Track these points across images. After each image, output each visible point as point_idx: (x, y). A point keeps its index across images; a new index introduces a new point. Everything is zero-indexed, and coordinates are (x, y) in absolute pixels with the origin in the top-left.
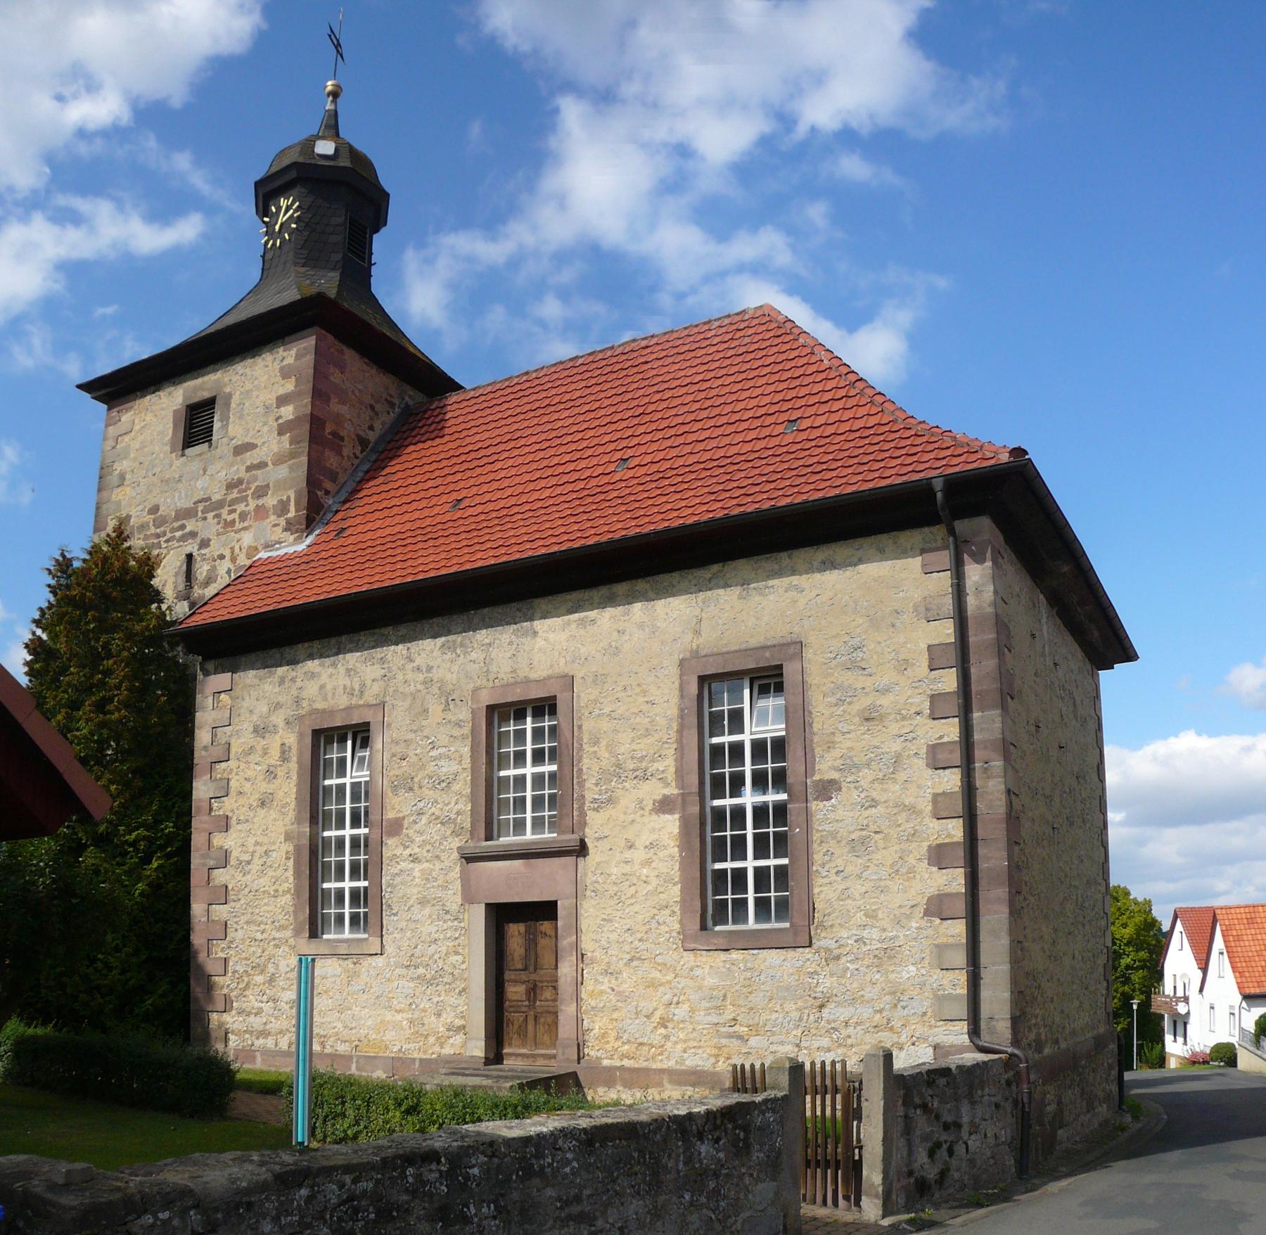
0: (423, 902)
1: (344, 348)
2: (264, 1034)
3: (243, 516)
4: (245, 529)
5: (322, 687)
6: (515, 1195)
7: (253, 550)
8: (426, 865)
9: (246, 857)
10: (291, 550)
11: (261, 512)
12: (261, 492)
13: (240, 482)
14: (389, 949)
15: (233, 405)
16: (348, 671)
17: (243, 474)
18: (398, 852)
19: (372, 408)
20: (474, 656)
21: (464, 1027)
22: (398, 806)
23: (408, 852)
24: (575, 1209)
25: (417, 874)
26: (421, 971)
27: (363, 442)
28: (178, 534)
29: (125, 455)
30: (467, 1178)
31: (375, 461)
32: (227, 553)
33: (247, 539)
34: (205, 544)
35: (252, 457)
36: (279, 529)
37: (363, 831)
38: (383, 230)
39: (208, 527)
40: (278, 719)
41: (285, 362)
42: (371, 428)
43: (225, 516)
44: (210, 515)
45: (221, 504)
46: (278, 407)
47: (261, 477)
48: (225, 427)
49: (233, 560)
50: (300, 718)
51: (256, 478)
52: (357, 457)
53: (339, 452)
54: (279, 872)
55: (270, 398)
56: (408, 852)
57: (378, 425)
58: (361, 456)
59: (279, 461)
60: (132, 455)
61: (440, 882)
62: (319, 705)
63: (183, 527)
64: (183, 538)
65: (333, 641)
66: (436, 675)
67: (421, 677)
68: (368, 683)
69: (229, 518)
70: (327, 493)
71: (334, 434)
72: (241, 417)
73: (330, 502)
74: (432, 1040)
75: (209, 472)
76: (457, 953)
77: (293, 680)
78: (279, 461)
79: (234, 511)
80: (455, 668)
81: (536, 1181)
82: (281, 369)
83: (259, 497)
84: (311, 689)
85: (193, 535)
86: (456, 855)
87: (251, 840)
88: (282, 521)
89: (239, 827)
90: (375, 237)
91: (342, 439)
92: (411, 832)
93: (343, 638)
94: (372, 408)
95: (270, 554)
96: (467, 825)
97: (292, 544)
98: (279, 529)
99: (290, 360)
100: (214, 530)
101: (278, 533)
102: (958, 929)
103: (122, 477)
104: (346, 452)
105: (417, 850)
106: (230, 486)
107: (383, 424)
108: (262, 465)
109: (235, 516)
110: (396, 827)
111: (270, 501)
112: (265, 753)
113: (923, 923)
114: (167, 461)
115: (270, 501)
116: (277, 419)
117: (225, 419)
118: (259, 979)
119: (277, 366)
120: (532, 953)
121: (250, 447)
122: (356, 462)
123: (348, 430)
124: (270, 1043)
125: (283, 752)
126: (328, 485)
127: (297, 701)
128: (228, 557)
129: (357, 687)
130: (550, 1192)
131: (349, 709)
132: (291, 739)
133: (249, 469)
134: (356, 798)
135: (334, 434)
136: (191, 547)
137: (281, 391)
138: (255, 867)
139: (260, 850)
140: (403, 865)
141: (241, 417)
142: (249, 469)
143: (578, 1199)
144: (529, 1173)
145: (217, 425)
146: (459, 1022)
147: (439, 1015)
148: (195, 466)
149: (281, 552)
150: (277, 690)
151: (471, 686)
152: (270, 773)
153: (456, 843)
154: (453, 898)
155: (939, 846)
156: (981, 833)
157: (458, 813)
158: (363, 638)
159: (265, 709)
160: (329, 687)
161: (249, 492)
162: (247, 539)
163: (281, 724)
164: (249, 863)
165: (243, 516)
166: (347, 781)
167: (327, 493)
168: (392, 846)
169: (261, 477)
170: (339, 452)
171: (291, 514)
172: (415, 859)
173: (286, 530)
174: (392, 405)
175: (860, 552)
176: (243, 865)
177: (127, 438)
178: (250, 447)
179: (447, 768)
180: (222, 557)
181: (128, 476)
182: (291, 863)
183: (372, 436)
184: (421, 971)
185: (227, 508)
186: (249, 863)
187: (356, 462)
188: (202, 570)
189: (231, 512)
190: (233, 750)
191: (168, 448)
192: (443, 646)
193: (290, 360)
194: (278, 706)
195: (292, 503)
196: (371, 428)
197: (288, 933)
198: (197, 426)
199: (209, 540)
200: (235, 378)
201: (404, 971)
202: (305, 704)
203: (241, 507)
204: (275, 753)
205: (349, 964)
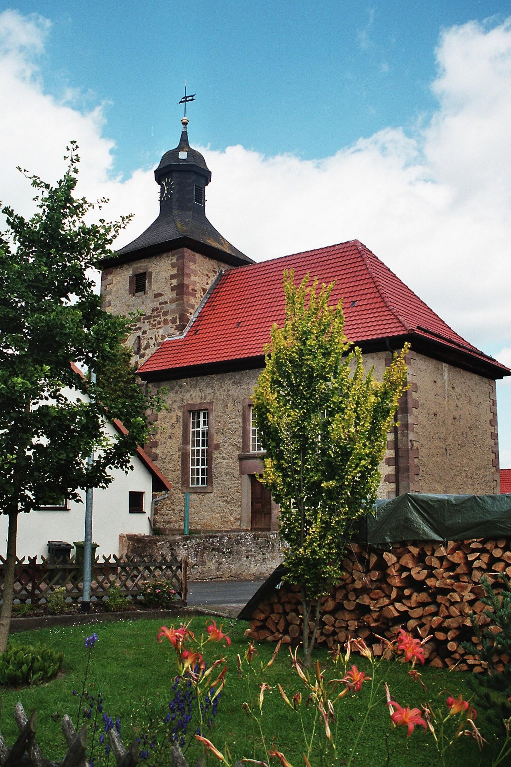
0: (226, 474)
1: (196, 254)
2: (170, 522)
3: (159, 323)
4: (160, 328)
5: (191, 395)
6: (235, 548)
7: (163, 337)
8: (227, 460)
9: (164, 457)
10: (178, 338)
11: (166, 322)
12: (166, 314)
13: (157, 308)
14: (215, 491)
15: (153, 277)
16: (200, 390)
17: (158, 306)
18: (218, 455)
19: (207, 275)
20: (243, 387)
21: (240, 519)
22: (217, 439)
23: (221, 456)
24: (250, 553)
25: (224, 463)
26: (226, 498)
27: (204, 290)
28: (134, 328)
29: (110, 293)
30: (224, 542)
31: (209, 298)
32: (153, 337)
33: (161, 332)
34: (144, 332)
35: (161, 299)
36: (173, 329)
37: (206, 448)
38: (210, 184)
39: (146, 326)
40: (175, 406)
41: (173, 261)
42: (207, 284)
43: (152, 322)
44: (146, 321)
45: (150, 317)
46: (171, 279)
47: (166, 307)
48: (150, 285)
49: (156, 340)
50: (183, 406)
51: (163, 308)
52: (202, 297)
53: (195, 296)
54: (176, 463)
55: (168, 275)
56: (221, 456)
57: (210, 282)
58: (203, 296)
59: (172, 301)
60: (113, 294)
61: (232, 467)
62: (190, 402)
63: (136, 325)
64: (136, 329)
65: (195, 378)
66: (230, 393)
67: (225, 394)
68: (207, 395)
69: (154, 323)
70: (191, 314)
71: (193, 290)
72: (157, 282)
73: (192, 317)
74: (229, 523)
75: (145, 304)
76: (238, 492)
77: (181, 392)
78: (172, 301)
79: (156, 320)
80: (237, 391)
81: (240, 545)
82: (171, 264)
83: (165, 315)
84: (187, 396)
85: (140, 328)
86: (237, 458)
87: (166, 451)
88: (174, 326)
89: (162, 446)
90: (206, 187)
91: (196, 291)
92: (222, 449)
93: (199, 378)
94: (207, 275)
95: (170, 339)
96: (241, 446)
97: (178, 336)
98: (173, 329)
99: (175, 261)
100: (148, 327)
101: (172, 331)
102: (393, 486)
103: (110, 302)
104: (197, 296)
105: (225, 455)
106: (153, 310)
107: (212, 281)
108: (166, 303)
109: (156, 322)
110: (217, 447)
111: (169, 318)
112: (171, 418)
113: (384, 484)
114: (127, 298)
115: (169, 318)
116: (171, 284)
117: (150, 282)
118: (169, 502)
119: (169, 262)
120: (152, 524)
121: (161, 295)
122: (202, 299)
123: (198, 287)
124: (172, 526)
125: (177, 418)
126: (191, 311)
127: (182, 400)
128: (154, 339)
129: (203, 396)
130: (243, 548)
131: (200, 404)
132: (180, 414)
133: (160, 304)
134: (203, 436)
135: (193, 290)
136: (139, 333)
137: (172, 273)
138: (166, 461)
139: (169, 454)
140: (220, 460)
141: (157, 282)
142: (160, 304)
143: (251, 551)
144: (238, 544)
145: (147, 285)
146: (238, 517)
147: (231, 514)
148: (139, 300)
149: (174, 339)
150: (175, 395)
151: (243, 398)
152: (173, 426)
153: (238, 453)
154: (237, 473)
155: (389, 458)
156: (400, 454)
157: (238, 442)
158: (205, 378)
159: (170, 402)
160: (193, 395)
161: (161, 313)
162: (161, 332)
163: (177, 408)
164: (165, 459)
165: (159, 323)
166: (200, 429)
167: (191, 314)
168: (216, 454)
169: (166, 307)
170: (195, 296)
171: (178, 324)
172: (224, 458)
173: (175, 329)
174: (215, 272)
175: (366, 359)
176: (163, 460)
177: (110, 286)
178: (161, 295)
179: (234, 426)
180: (151, 338)
181: (112, 303)
182: (180, 459)
183: (208, 287)
184: (226, 498)
185: (153, 319)
186: (165, 459)
187: (202, 299)
188: (144, 343)
189: (154, 321)
190: (159, 417)
191: (128, 292)
192: (233, 383)
193: (175, 261)
194: (175, 401)
195: (178, 319)
196: (207, 284)
197: (179, 485)
198: (139, 284)
199: (146, 331)
200: (153, 266)
201: (220, 499)
202: (185, 401)
203: (158, 319)
204: (174, 420)
205: (200, 496)
